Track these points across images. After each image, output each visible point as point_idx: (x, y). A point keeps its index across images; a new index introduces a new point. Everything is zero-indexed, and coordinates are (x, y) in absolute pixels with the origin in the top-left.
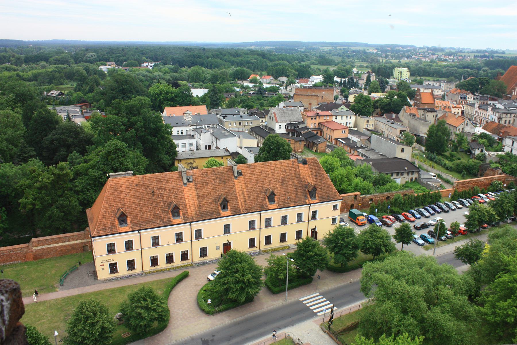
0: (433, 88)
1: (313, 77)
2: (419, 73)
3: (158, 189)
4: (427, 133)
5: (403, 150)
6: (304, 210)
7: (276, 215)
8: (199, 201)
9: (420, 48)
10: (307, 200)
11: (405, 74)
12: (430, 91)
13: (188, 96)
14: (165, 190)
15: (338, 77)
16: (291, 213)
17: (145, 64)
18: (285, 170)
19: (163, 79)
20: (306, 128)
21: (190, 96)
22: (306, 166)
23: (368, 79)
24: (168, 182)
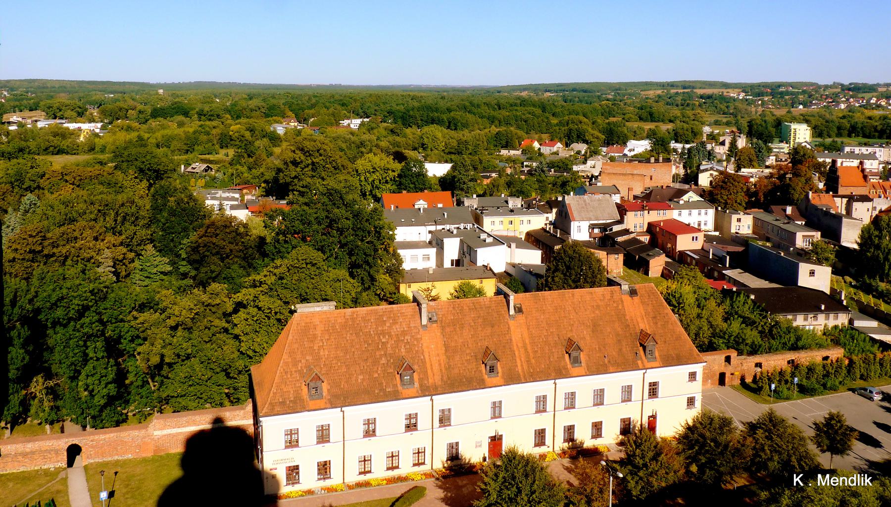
0: (862, 158)
1: (632, 143)
2: (835, 130)
3: (379, 335)
4: (859, 240)
5: (812, 273)
6: (634, 378)
7: (583, 385)
8: (448, 358)
9: (826, 87)
10: (639, 362)
11: (802, 134)
12: (856, 163)
14: (390, 336)
15: (677, 141)
17: (346, 122)
18: (598, 306)
19: (377, 146)
20: (626, 232)
21: (422, 175)
22: (636, 299)
23: (733, 144)
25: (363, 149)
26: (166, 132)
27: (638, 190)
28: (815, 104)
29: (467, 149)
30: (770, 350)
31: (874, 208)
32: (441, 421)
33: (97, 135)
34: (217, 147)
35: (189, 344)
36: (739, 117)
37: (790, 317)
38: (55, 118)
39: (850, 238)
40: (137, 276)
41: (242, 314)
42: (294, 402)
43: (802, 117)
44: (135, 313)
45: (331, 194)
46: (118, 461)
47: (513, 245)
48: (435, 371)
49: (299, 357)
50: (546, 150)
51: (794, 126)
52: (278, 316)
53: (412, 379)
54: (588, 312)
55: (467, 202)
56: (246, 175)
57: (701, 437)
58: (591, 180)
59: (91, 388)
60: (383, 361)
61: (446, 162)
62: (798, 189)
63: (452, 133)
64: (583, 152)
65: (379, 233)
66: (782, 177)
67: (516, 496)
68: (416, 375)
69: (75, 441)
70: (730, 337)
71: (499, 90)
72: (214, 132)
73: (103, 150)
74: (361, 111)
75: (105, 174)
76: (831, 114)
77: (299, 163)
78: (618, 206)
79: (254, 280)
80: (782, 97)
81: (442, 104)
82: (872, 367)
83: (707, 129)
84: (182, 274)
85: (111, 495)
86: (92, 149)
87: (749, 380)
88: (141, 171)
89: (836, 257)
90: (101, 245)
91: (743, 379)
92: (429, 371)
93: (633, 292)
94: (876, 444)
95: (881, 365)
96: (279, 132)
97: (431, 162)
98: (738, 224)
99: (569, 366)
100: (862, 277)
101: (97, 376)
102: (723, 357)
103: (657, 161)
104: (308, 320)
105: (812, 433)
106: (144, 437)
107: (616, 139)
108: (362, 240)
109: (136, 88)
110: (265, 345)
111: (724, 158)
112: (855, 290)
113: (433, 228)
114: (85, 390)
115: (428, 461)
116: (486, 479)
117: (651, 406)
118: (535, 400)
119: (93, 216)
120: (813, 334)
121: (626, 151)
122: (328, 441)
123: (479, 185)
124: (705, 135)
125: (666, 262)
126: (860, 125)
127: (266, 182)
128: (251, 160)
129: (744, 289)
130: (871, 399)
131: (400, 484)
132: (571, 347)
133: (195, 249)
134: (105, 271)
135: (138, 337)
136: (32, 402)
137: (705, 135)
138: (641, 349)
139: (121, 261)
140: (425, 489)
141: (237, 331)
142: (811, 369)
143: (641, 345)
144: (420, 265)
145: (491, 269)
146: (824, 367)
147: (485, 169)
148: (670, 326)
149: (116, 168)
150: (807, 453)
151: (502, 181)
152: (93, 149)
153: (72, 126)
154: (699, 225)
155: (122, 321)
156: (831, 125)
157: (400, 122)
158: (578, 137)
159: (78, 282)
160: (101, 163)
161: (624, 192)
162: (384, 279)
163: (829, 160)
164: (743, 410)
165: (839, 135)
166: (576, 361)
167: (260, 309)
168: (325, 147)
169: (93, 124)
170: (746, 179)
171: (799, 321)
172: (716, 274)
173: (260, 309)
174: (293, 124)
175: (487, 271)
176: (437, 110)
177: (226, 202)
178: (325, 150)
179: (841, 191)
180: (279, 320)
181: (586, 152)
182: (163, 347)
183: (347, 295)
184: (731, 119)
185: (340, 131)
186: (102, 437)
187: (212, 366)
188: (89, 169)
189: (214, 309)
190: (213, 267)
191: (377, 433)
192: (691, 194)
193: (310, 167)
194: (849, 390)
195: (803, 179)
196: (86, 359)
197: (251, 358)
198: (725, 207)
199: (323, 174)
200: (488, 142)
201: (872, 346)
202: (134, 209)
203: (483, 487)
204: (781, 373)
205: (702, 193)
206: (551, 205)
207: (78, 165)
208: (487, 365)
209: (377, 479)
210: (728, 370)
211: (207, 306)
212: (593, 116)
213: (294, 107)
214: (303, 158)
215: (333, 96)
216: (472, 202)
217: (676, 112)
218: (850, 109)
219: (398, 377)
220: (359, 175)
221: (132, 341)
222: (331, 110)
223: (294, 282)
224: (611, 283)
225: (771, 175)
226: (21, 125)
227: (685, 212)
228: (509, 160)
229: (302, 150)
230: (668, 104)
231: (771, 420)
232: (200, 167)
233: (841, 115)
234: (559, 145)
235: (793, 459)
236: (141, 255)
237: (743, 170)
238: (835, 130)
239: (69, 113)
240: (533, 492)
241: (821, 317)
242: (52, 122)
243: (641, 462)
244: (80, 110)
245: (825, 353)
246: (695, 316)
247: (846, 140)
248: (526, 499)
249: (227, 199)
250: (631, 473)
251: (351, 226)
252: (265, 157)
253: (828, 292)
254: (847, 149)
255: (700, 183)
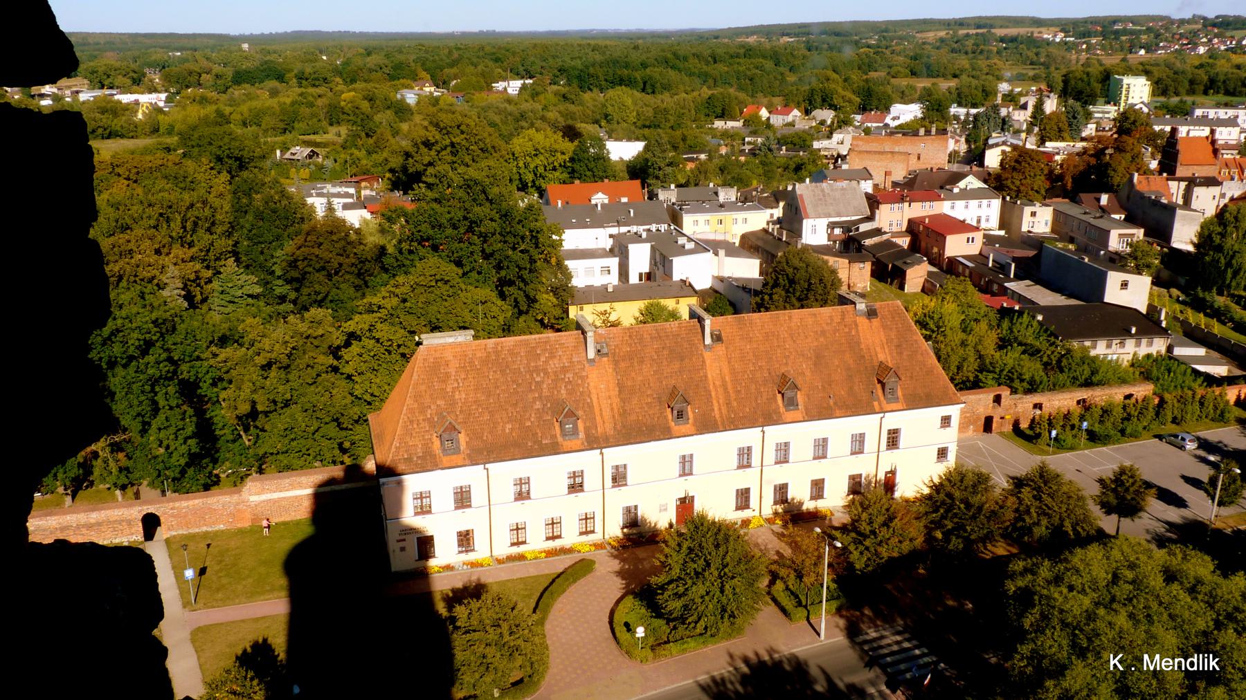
1: (897, 109)
5: (1124, 285)
6: (867, 424)
7: (800, 434)
9: (1182, 22)
10: (876, 404)
11: (1138, 91)
12: (1206, 132)
13: (599, 159)
14: (546, 373)
15: (960, 105)
16: (839, 430)
17: (500, 86)
18: (823, 333)
19: (543, 118)
20: (878, 232)
21: (602, 158)
22: (875, 322)
23: (1039, 107)
24: (552, 356)
25: (524, 124)
26: (254, 104)
27: (899, 174)
28: (1163, 48)
29: (667, 120)
30: (1054, 387)
31: (1223, 196)
32: (614, 479)
33: (160, 110)
34: (325, 123)
35: (288, 386)
36: (1052, 69)
37: (1088, 343)
38: (102, 87)
39: (1184, 237)
40: (215, 301)
41: (355, 348)
42: (423, 458)
43: (1141, 67)
44: (213, 348)
45: (469, 186)
46: (207, 533)
47: (722, 252)
48: (606, 418)
49: (427, 400)
50: (777, 120)
51: (1127, 80)
52: (402, 350)
53: (575, 427)
54: (809, 340)
55: (662, 195)
56: (364, 162)
57: (953, 498)
58: (836, 161)
59: (165, 443)
60: (538, 405)
61: (638, 139)
62: (1121, 169)
63: (648, 98)
64: (829, 122)
65: (537, 238)
66: (1099, 153)
67: (704, 570)
68: (580, 424)
69: (151, 509)
70: (1002, 371)
71: (716, 35)
72: (320, 102)
73: (170, 131)
74: (521, 69)
75: (170, 164)
76: (1184, 61)
77: (433, 144)
78: (869, 197)
79: (371, 304)
80: (1117, 39)
81: (635, 57)
82: (1190, 407)
83: (1004, 87)
84: (279, 297)
85: (203, 571)
86: (155, 130)
87: (1024, 425)
88: (219, 159)
89: (1161, 262)
90: (166, 260)
91: (1016, 424)
92: (598, 419)
93: (871, 313)
94: (1179, 502)
95: (1202, 404)
96: (408, 101)
97: (617, 140)
98: (1032, 219)
99: (782, 409)
100: (1194, 289)
101: (172, 430)
102: (991, 396)
103: (928, 132)
104: (438, 355)
105: (1096, 489)
106: (238, 504)
107: (875, 103)
108: (514, 249)
109: (212, 42)
110: (386, 387)
111: (1025, 127)
112: (1183, 307)
113: (614, 231)
114: (160, 446)
115: (598, 528)
116: (667, 550)
117: (889, 460)
118: (736, 452)
119: (152, 222)
120: (1115, 366)
121: (888, 120)
122: (470, 506)
123: (680, 170)
124: (1000, 95)
125: (930, 273)
126: (1222, 78)
127: (392, 171)
128: (371, 141)
129: (1031, 306)
130: (1182, 448)
131: (563, 557)
132: (785, 386)
133: (293, 264)
134: (172, 294)
135: (221, 379)
136: (94, 463)
137: (1000, 95)
138: (877, 387)
139: (194, 281)
140: (593, 562)
141: (348, 369)
142: (1106, 412)
143: (879, 381)
144: (598, 280)
145: (690, 285)
146: (1124, 408)
147: (691, 149)
148: (920, 358)
149: (185, 155)
150: (1086, 516)
151: (712, 166)
152: (157, 130)
153: (126, 98)
154: (979, 221)
155: (198, 359)
156: (1180, 77)
157: (575, 83)
158: (824, 100)
159: (134, 310)
160: (168, 150)
161: (879, 178)
162: (547, 300)
163: (1168, 129)
164: (1007, 462)
165: (1191, 92)
166: (791, 403)
167: (378, 340)
168: (468, 121)
169: (154, 95)
170: (1050, 156)
171: (1100, 349)
172: (995, 287)
173: (378, 340)
174: (429, 89)
175: (686, 288)
176: (627, 66)
177: (335, 201)
178: (468, 125)
179: (1181, 171)
180: (403, 355)
181: (833, 123)
182: (254, 391)
183: (493, 322)
184: (1041, 71)
185: (492, 98)
186: (184, 504)
187: (319, 414)
188: (149, 158)
189: (316, 343)
190: (317, 287)
191: (532, 495)
192: (970, 178)
193: (449, 149)
194: (1155, 436)
195: (1128, 156)
196: (156, 410)
197: (369, 403)
198: (1017, 196)
199: (467, 159)
200: (697, 110)
201: (1195, 380)
202: (207, 212)
203: (663, 559)
204: (1067, 416)
205: (987, 178)
206: (777, 197)
207: (133, 153)
208: (671, 409)
209: (533, 551)
210: (997, 413)
211: (307, 338)
212: (850, 71)
213: (428, 64)
214: (438, 137)
215: (482, 48)
216: (669, 195)
217: (963, 62)
218: (1212, 54)
219: (557, 425)
220: (516, 159)
221: (214, 384)
222: (480, 68)
223: (420, 305)
224: (843, 301)
225: (1085, 150)
226: (55, 98)
227: (960, 204)
228: (726, 134)
229: (437, 125)
230: (953, 51)
231: (1041, 476)
232: (301, 152)
233: (1197, 63)
234: (796, 112)
235: (1067, 524)
236: (220, 273)
237: (1048, 144)
238: (1186, 84)
239: (120, 80)
240: (725, 566)
241: (1130, 344)
242: (98, 93)
243: (868, 528)
244: (135, 76)
245: (1127, 390)
246: (958, 343)
247: (1200, 99)
248: (716, 574)
249: (338, 195)
250: (855, 542)
251: (498, 230)
252: (390, 138)
253: (1144, 311)
254: (1199, 112)
255: (986, 163)
